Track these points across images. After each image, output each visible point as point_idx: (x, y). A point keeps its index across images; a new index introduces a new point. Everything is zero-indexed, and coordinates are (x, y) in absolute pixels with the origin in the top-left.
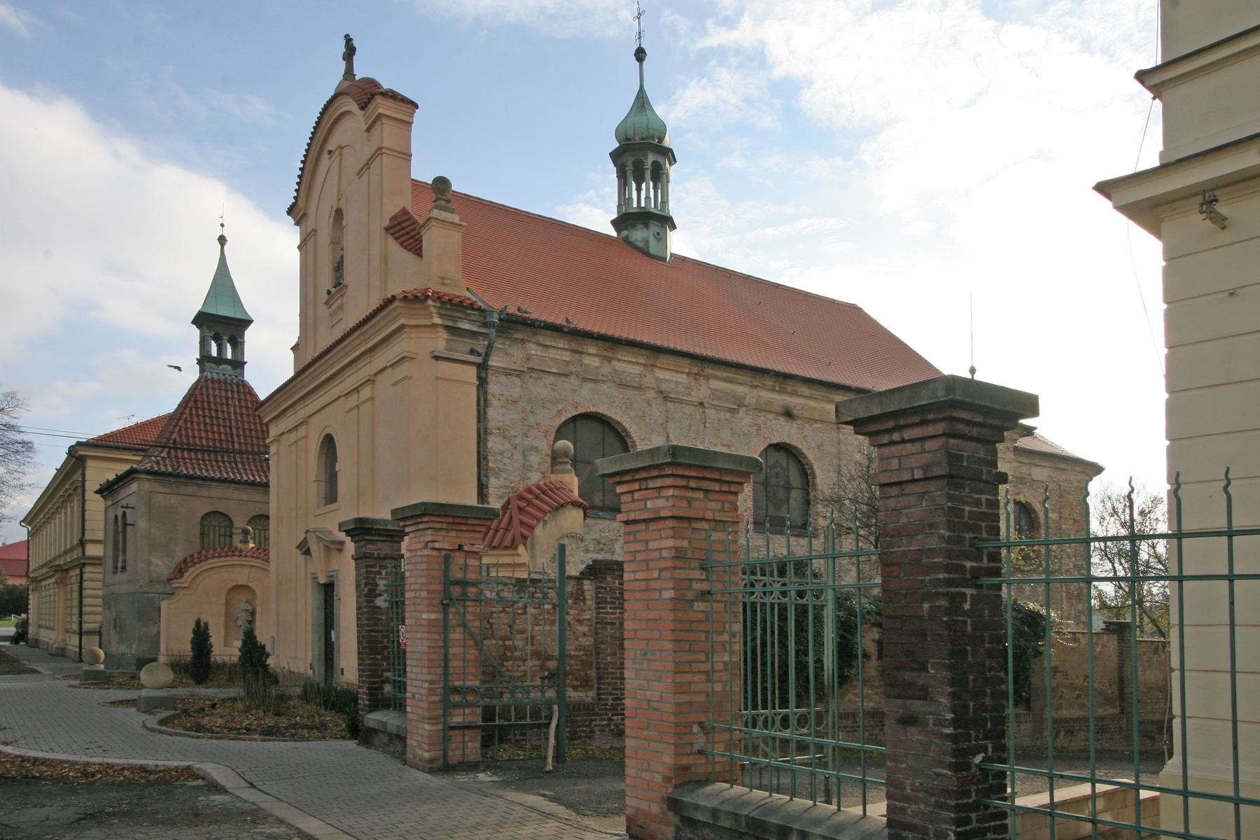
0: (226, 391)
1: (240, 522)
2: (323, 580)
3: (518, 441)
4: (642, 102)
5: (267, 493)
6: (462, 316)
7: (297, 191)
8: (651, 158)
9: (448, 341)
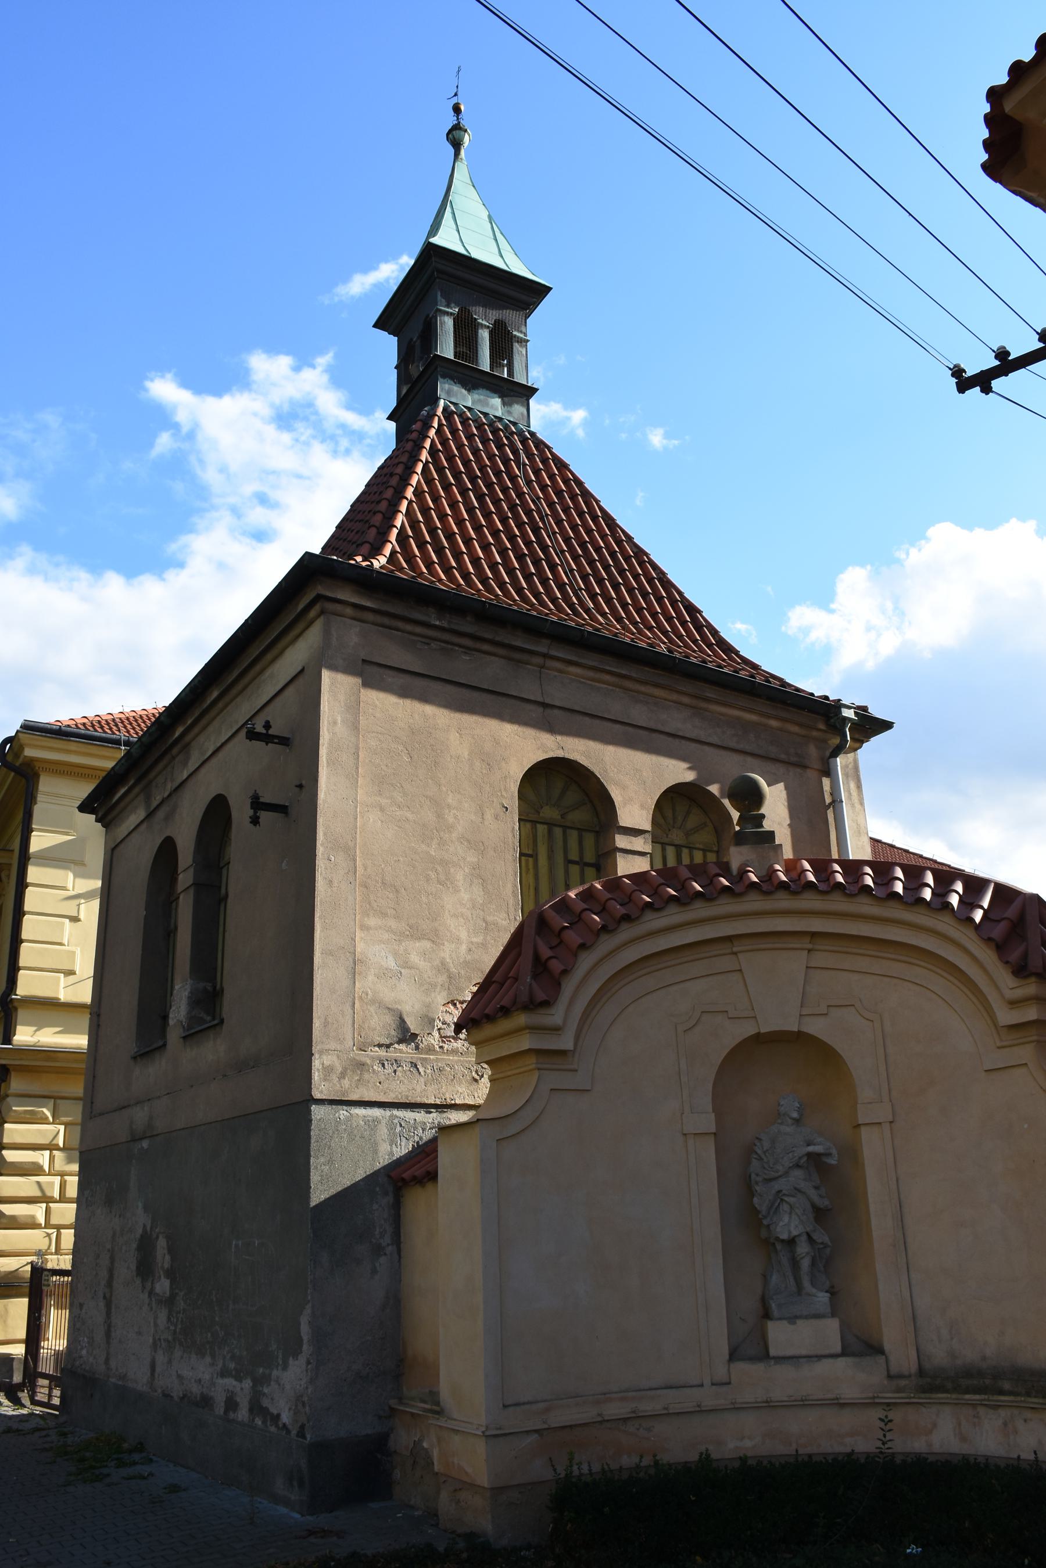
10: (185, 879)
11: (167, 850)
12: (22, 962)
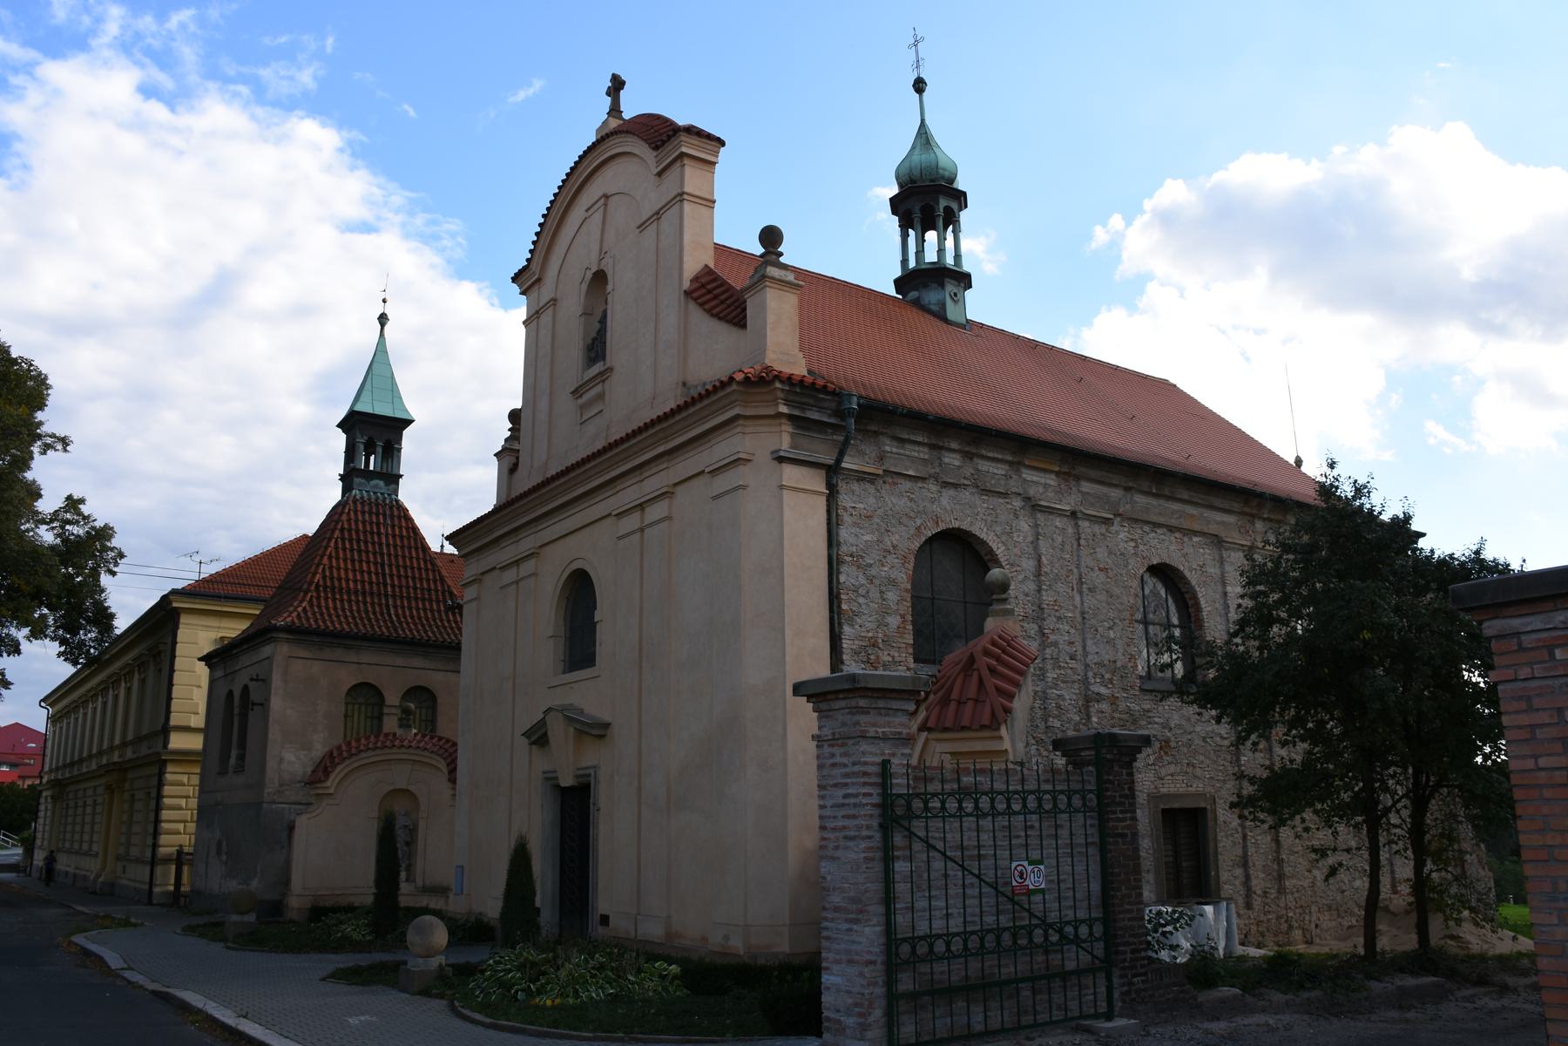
0: (378, 514)
1: (392, 698)
2: (567, 781)
3: (873, 572)
4: (924, 137)
5: (458, 658)
6: (811, 401)
7: (531, 251)
8: (943, 203)
9: (793, 435)
10: (236, 711)
11: (231, 693)
12: (173, 708)
